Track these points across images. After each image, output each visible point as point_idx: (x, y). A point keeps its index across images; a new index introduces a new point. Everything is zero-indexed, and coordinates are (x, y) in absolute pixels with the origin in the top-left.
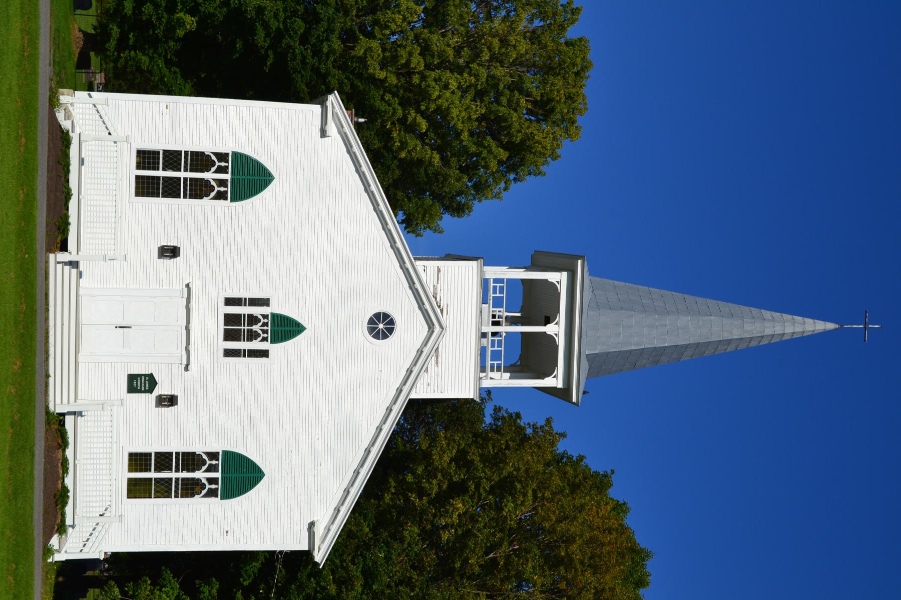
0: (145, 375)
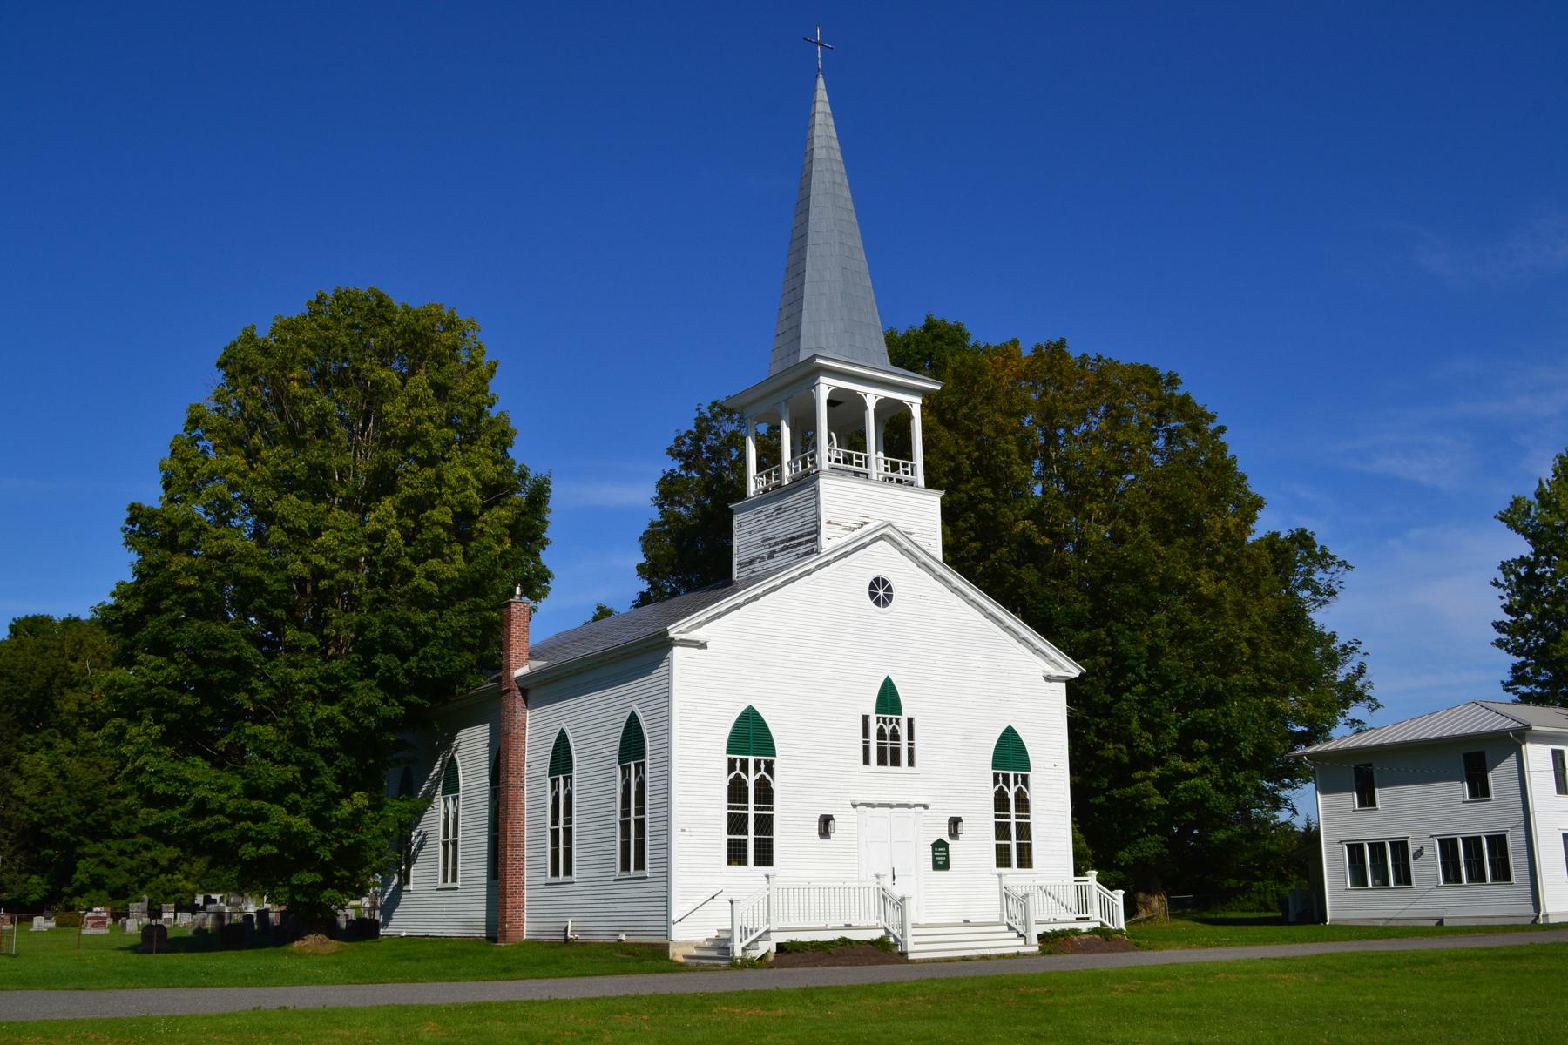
0: (934, 851)
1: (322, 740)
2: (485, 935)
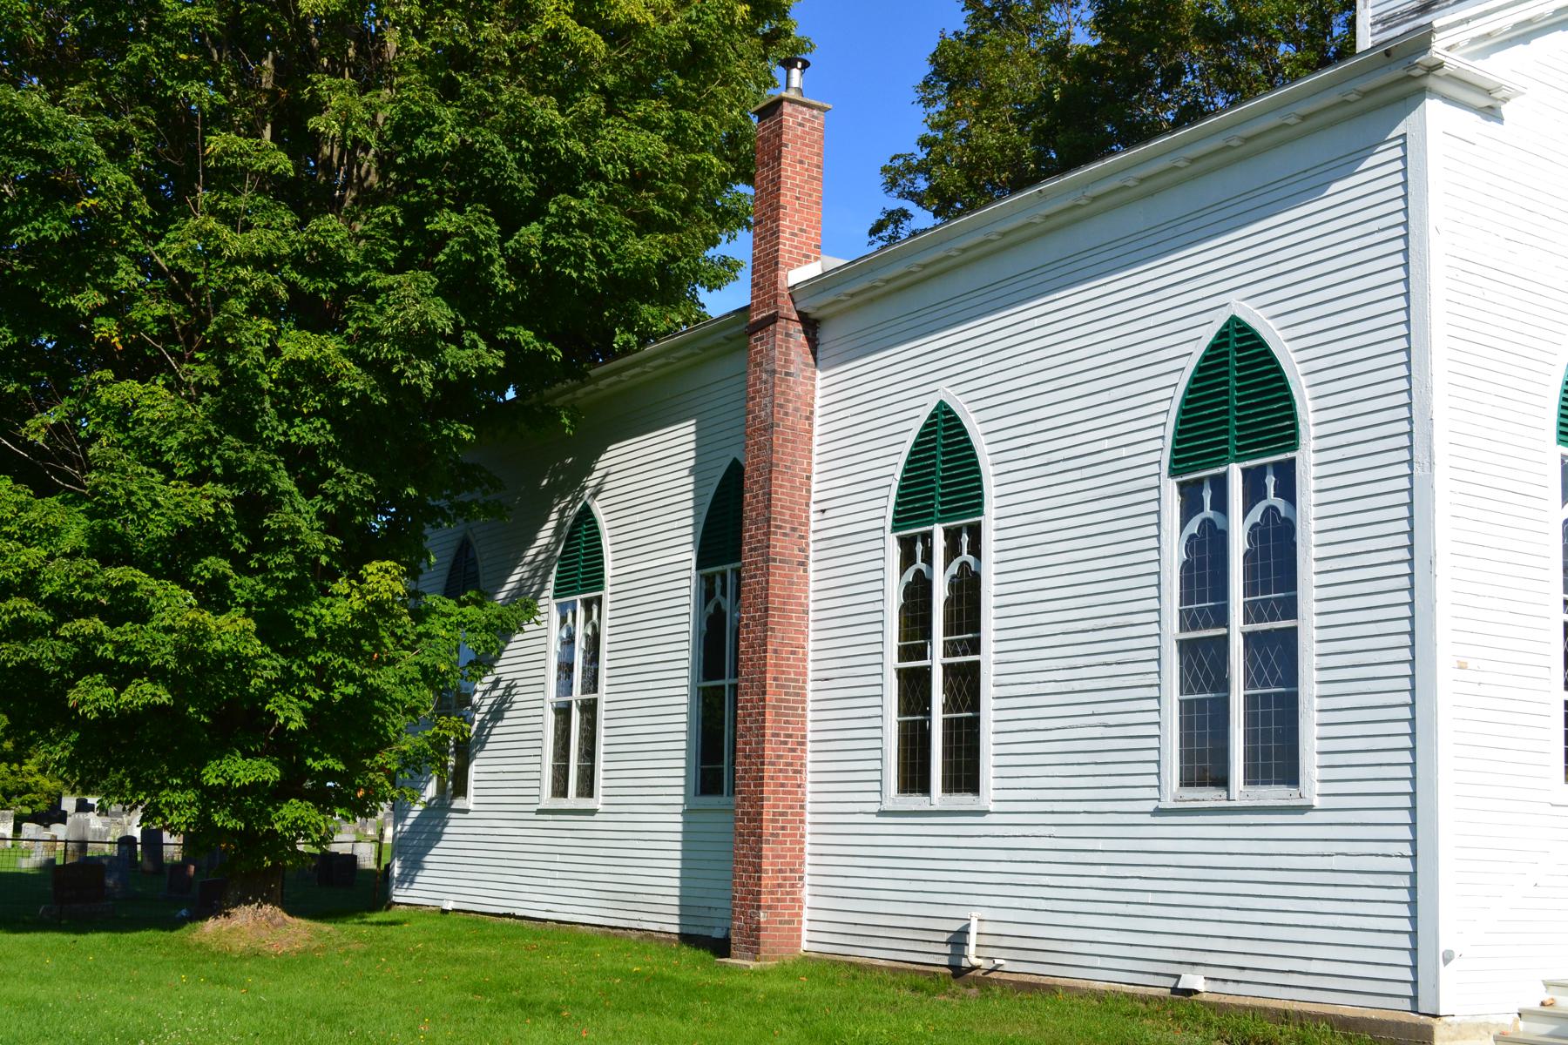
1: (291, 425)
2: (676, 929)
